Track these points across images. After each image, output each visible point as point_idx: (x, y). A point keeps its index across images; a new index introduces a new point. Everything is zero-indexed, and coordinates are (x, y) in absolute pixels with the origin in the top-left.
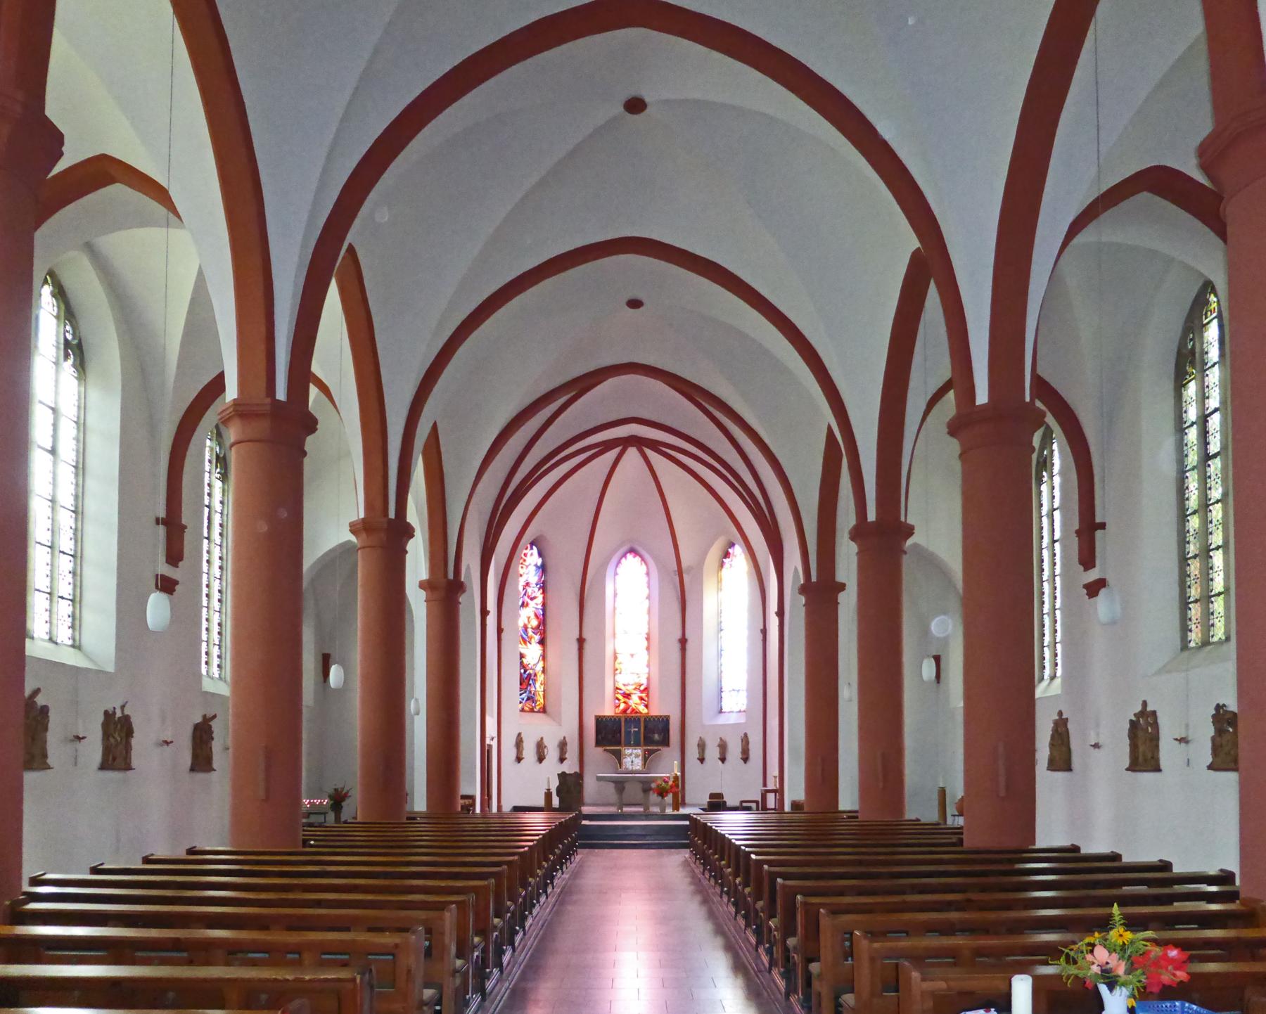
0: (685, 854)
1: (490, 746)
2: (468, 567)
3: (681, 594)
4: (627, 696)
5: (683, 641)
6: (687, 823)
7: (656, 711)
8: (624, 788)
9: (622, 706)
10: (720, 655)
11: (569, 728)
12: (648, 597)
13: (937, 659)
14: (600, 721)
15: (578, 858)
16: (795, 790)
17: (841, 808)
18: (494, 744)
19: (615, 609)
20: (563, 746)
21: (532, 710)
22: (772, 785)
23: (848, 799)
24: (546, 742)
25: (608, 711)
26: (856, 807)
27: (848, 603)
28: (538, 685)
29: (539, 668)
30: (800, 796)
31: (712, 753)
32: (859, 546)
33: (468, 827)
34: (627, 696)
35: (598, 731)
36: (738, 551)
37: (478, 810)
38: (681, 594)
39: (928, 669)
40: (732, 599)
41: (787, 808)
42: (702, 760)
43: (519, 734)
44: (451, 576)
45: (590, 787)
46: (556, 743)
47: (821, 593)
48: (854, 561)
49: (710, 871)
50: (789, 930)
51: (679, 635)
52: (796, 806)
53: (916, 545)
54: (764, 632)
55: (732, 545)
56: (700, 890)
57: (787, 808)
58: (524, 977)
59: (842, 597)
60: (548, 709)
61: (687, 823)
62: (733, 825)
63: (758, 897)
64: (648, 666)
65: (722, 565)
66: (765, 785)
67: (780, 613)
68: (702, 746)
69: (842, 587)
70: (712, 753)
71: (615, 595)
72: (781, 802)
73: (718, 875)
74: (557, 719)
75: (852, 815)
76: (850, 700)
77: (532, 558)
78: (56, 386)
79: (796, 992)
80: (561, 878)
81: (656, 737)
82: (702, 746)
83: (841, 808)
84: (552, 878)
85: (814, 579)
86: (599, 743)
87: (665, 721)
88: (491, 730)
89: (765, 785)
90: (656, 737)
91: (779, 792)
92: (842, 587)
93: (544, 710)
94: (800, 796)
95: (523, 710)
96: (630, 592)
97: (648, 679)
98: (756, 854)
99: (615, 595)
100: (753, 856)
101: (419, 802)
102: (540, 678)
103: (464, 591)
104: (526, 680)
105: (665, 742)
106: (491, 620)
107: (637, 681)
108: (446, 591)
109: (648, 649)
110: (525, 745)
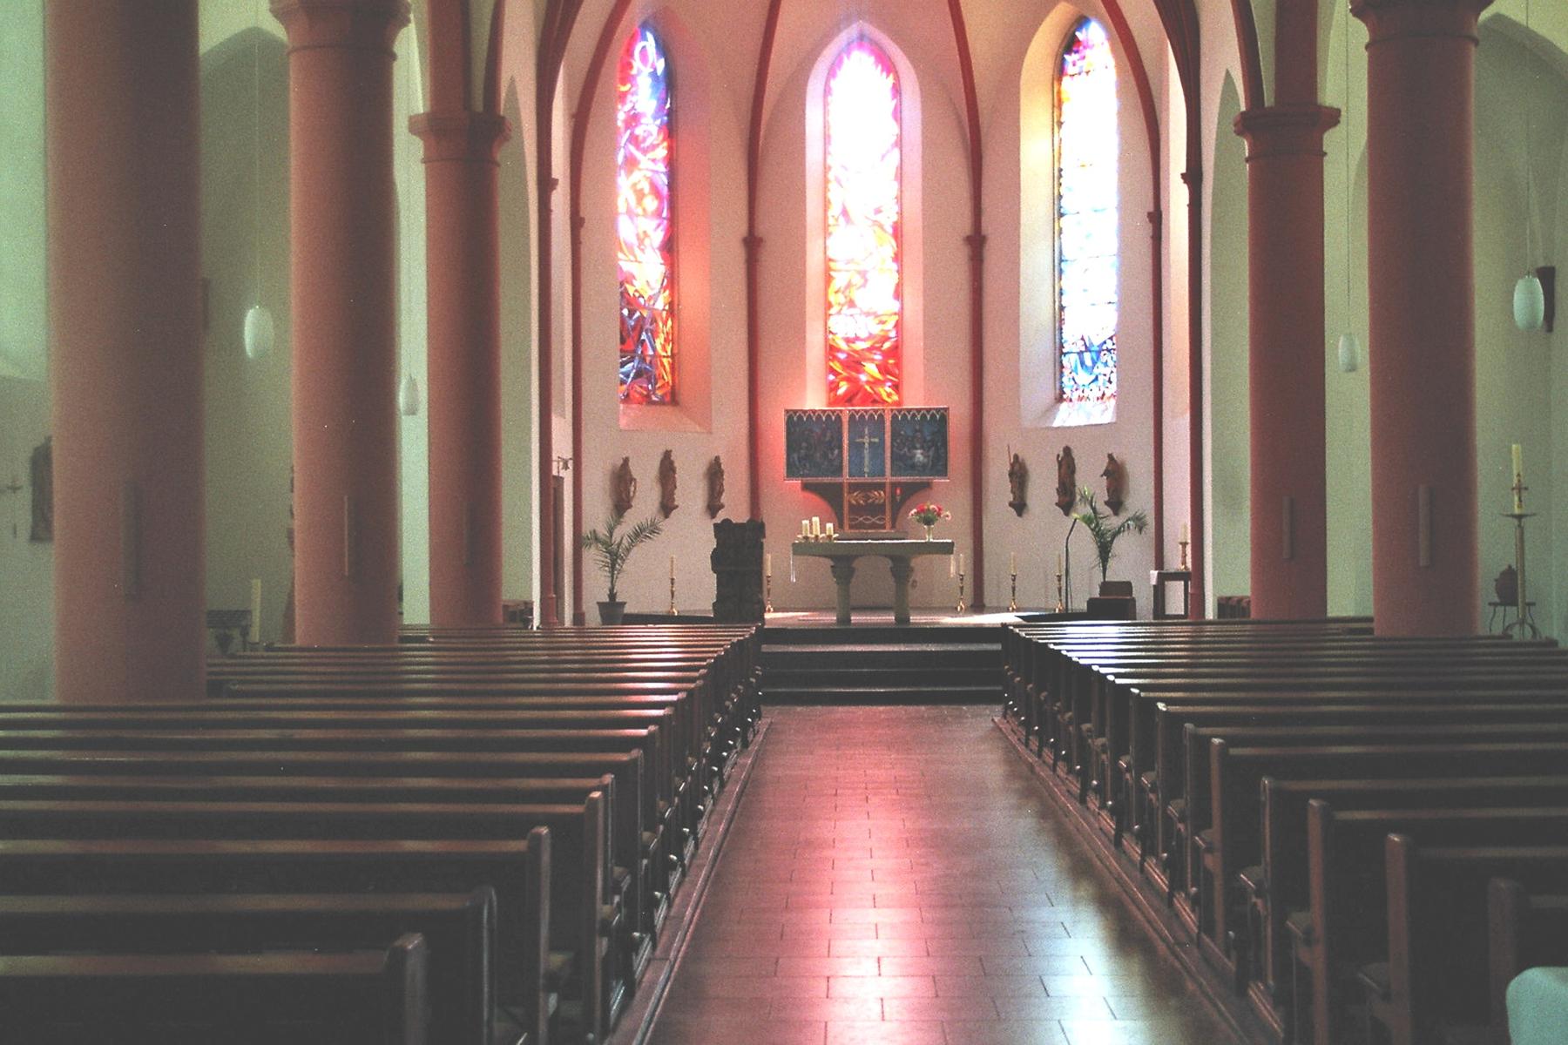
0: (992, 715)
1: (559, 480)
2: (512, 80)
3: (971, 139)
4: (854, 363)
5: (976, 242)
6: (997, 647)
7: (916, 398)
8: (852, 571)
9: (843, 387)
10: (1058, 272)
11: (725, 436)
12: (899, 143)
13: (1547, 276)
14: (798, 423)
15: (762, 725)
16: (1230, 572)
17: (1333, 611)
18: (568, 476)
19: (826, 169)
20: (715, 474)
21: (647, 399)
22: (1176, 560)
23: (1349, 586)
24: (635, 470)
25: (814, 400)
26: (1369, 612)
27: (1345, 158)
28: (659, 342)
29: (661, 304)
30: (1241, 585)
31: (1043, 487)
32: (1372, 31)
33: (519, 655)
34: (854, 363)
35: (791, 446)
36: (1095, 34)
37: (536, 622)
38: (971, 139)
39: (1526, 297)
40: (1077, 140)
41: (1210, 614)
42: (1020, 506)
43: (667, 454)
44: (479, 106)
45: (777, 562)
46: (701, 467)
47: (1282, 129)
48: (1361, 59)
49: (1055, 748)
50: (1240, 853)
51: (966, 227)
52: (1228, 607)
53: (1498, 18)
54: (1156, 218)
55: (1081, 21)
56: (1030, 790)
57: (1210, 614)
58: (696, 952)
59: (1332, 140)
60: (685, 395)
61: (997, 647)
62: (1094, 645)
63: (1172, 792)
64: (898, 294)
65: (1060, 71)
66: (1159, 563)
67: (1193, 177)
68: (1019, 474)
69: (1332, 117)
70: (1043, 487)
71: (827, 139)
72: (1195, 599)
73: (1079, 757)
74: (705, 422)
75: (1356, 627)
76: (1352, 368)
77: (647, 61)
78: (1522, 540)
79: (1260, 975)
80: (737, 765)
81: (919, 455)
82: (1019, 474)
83: (1333, 611)
84: (721, 762)
85: (1269, 99)
86: (792, 471)
87: (937, 422)
88: (562, 445)
89: (1159, 563)
90: (919, 455)
91: (1194, 578)
92: (1332, 117)
93: (673, 398)
94: (1241, 585)
95: (627, 398)
96: (859, 128)
97: (898, 326)
98: (1167, 701)
99: (827, 139)
100: (1161, 706)
101: (417, 608)
102: (665, 328)
103: (507, 139)
104: (631, 336)
105: (939, 465)
106: (560, 200)
107: (877, 330)
108: (469, 134)
109: (898, 258)
110: (680, 476)
